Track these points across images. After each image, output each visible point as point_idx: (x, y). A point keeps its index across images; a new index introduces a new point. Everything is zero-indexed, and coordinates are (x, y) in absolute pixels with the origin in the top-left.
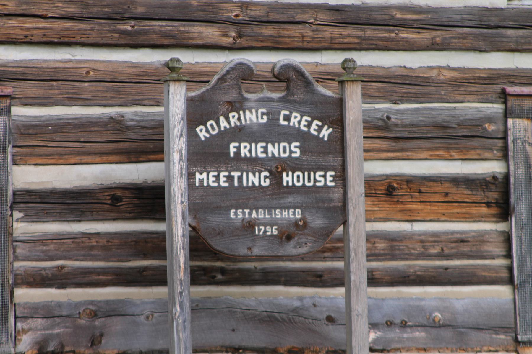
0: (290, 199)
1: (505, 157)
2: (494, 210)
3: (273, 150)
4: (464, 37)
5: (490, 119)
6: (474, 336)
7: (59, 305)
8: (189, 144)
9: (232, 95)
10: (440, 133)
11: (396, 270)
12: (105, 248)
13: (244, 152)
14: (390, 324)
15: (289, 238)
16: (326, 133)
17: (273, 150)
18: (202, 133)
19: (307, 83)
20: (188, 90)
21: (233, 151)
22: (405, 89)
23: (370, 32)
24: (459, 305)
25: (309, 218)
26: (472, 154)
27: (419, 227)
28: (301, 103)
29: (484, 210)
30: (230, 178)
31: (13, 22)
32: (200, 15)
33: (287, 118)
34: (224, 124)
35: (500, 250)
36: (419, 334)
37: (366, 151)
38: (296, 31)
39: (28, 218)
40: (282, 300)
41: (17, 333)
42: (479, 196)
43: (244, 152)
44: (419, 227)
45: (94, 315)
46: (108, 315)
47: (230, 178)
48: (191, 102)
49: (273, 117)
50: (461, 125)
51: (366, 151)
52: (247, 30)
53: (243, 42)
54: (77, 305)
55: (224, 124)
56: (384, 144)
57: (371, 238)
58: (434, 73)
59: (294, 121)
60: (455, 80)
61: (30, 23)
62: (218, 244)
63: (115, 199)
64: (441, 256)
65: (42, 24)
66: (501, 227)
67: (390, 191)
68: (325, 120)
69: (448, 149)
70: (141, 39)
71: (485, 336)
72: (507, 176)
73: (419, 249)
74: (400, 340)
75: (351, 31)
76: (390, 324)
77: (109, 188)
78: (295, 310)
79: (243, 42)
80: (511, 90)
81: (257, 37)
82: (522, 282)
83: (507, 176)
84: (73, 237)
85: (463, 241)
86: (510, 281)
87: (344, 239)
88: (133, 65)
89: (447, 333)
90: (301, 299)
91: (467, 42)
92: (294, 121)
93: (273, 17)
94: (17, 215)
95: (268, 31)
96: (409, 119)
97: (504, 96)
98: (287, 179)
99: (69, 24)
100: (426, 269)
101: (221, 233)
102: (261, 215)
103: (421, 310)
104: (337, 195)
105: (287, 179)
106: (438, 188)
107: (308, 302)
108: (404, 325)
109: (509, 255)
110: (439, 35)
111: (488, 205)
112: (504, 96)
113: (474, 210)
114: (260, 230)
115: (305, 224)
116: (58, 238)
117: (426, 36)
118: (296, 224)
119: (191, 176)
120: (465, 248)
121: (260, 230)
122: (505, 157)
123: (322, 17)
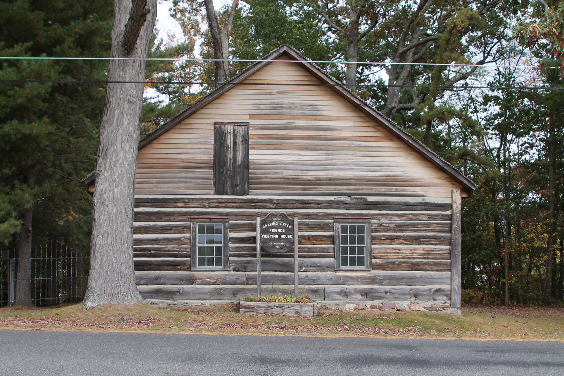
0: (282, 241)
1: (334, 231)
2: (331, 242)
3: (279, 230)
4: (325, 206)
5: (330, 223)
6: (326, 269)
7: (238, 261)
8: (261, 229)
9: (270, 219)
10: (319, 226)
11: (310, 255)
12: (248, 249)
13: (273, 231)
14: (308, 266)
15: (282, 248)
16: (290, 227)
17: (279, 230)
18: (264, 227)
19: (286, 217)
20: (261, 218)
21: (270, 230)
22: (312, 217)
23: (305, 205)
24: (323, 262)
25: (286, 244)
26: (327, 231)
27: (315, 246)
28: (285, 221)
29: (329, 242)
30: (270, 236)
31: (230, 204)
32: (268, 202)
33: (282, 224)
34: (268, 225)
35: (332, 251)
36: (314, 268)
37: (138, 266)
38: (289, 205)
39: (232, 243)
40: (284, 261)
41: (230, 266)
42: (328, 239)
43: (273, 231)
44: (315, 246)
45: (245, 263)
46: (248, 263)
47: (270, 236)
48: (261, 221)
49: (279, 224)
50: (324, 224)
51: (138, 266)
52: (278, 205)
53: (278, 207)
54: (242, 261)
55: (268, 225)
56: (307, 229)
57: (299, 248)
58: (318, 214)
59: (283, 225)
60: (323, 215)
61: (233, 204)
62: (267, 250)
63: (250, 240)
64: (319, 252)
65: (236, 204)
66: (333, 246)
67: (309, 238)
68: (290, 224)
69: (321, 230)
70: (256, 207)
71: (328, 269)
72: (334, 235)
73: (315, 251)
74: (310, 269)
75: (300, 205)
76: (308, 266)
77: (249, 237)
78: (288, 263)
79: (278, 207)
80: (335, 217)
81: (281, 206)
82: (336, 258)
83: (334, 235)
84: (241, 247)
85: (324, 249)
86: (334, 257)
87: (294, 248)
88: (255, 212)
89: (320, 268)
90: (289, 261)
91: (326, 207)
92: (283, 225)
93: (284, 202)
94: (230, 242)
95: (283, 205)
96: (313, 223)
97: (334, 219)
98: (282, 236)
99: (241, 204)
100: (316, 255)
101: (267, 247)
102: (276, 244)
103: (314, 263)
104: (292, 240)
105: (282, 236)
106: (319, 238)
107: (290, 261)
108: (311, 266)
109: (334, 252)
110: (319, 206)
111: (330, 241)
112: (334, 219)
113: (327, 242)
114: (276, 247)
115: (286, 246)
116: (238, 247)
117: (317, 206)
118: (283, 245)
119: (261, 236)
120: (325, 251)
121: (276, 247)
122: (334, 231)
123: (294, 202)
